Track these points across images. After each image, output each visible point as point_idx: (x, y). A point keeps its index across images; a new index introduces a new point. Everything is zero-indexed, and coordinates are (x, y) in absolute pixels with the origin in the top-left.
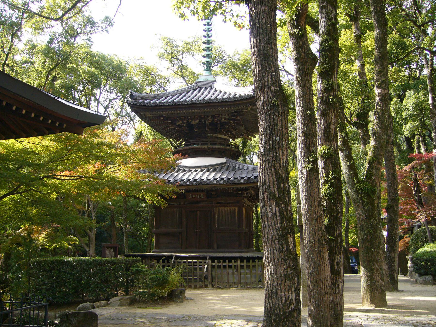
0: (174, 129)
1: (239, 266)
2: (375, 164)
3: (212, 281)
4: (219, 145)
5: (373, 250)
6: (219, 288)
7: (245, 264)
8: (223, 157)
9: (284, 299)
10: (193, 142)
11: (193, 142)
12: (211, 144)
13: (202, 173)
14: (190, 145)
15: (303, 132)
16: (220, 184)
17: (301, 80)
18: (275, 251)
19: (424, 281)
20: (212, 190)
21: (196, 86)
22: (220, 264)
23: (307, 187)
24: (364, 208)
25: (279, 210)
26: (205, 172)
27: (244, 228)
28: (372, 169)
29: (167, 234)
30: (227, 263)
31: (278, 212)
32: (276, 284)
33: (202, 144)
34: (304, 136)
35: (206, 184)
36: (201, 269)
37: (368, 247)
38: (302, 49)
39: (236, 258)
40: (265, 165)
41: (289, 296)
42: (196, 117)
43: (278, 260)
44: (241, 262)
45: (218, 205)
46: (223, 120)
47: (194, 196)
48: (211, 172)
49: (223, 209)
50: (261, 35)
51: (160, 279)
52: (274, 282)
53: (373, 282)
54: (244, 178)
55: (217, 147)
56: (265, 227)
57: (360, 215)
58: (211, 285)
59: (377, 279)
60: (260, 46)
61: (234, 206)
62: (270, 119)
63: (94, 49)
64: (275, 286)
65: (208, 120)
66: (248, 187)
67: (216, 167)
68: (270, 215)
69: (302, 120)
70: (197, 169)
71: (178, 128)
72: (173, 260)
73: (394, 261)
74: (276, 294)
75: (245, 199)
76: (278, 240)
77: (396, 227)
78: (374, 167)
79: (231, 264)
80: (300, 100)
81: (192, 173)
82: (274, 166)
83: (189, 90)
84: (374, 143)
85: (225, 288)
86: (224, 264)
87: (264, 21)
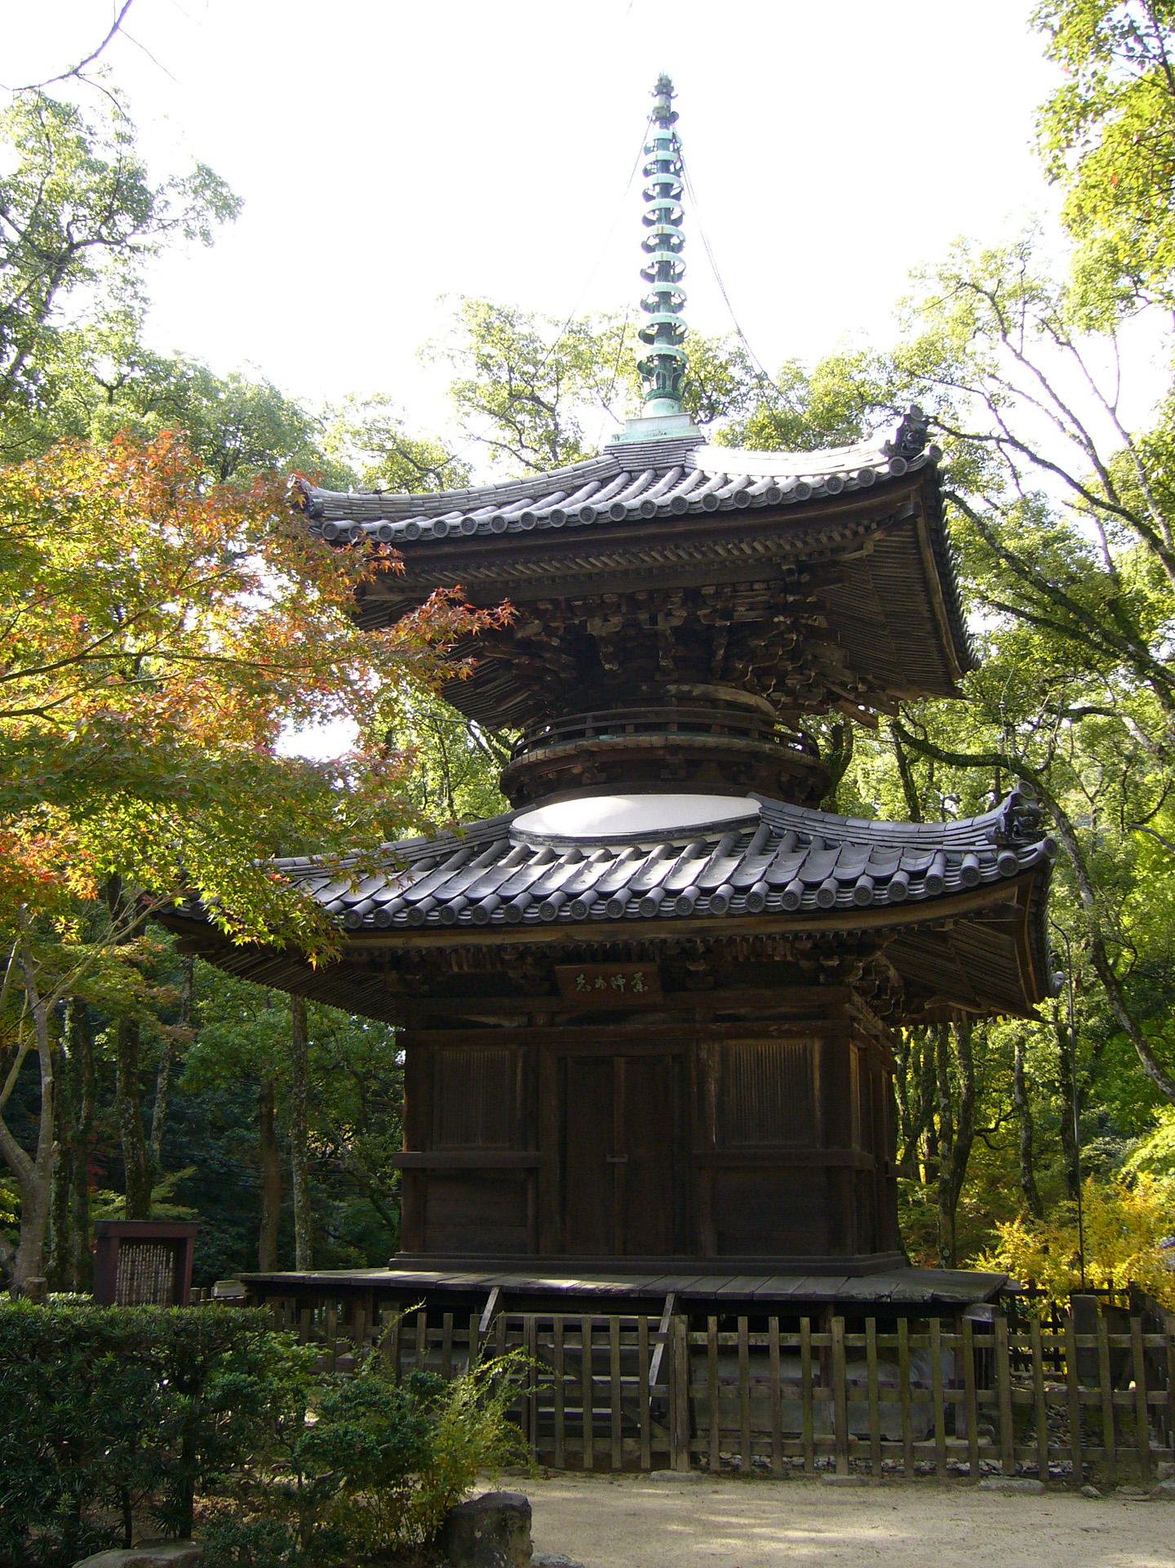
0: (507, 665)
1: (838, 1351)
3: (693, 1435)
4: (721, 734)
6: (732, 1473)
7: (869, 1339)
8: (743, 794)
10: (596, 719)
11: (596, 719)
12: (683, 727)
13: (637, 865)
14: (581, 734)
16: (730, 915)
20: (686, 952)
21: (608, 466)
22: (732, 1338)
26: (654, 861)
27: (856, 1147)
29: (464, 1176)
30: (773, 1336)
33: (641, 728)
35: (657, 918)
36: (633, 1363)
39: (817, 1310)
42: (610, 598)
44: (849, 1329)
45: (722, 1027)
46: (742, 612)
47: (600, 983)
48: (686, 861)
49: (745, 1049)
51: (366, 1452)
54: (855, 880)
55: (710, 740)
58: (685, 1457)
61: (800, 1034)
63: (157, 340)
65: (669, 614)
66: (878, 931)
67: (710, 839)
70: (614, 850)
71: (525, 660)
72: (487, 1314)
75: (857, 998)
79: (793, 1340)
81: (589, 866)
83: (578, 482)
85: (763, 1474)
86: (757, 1339)
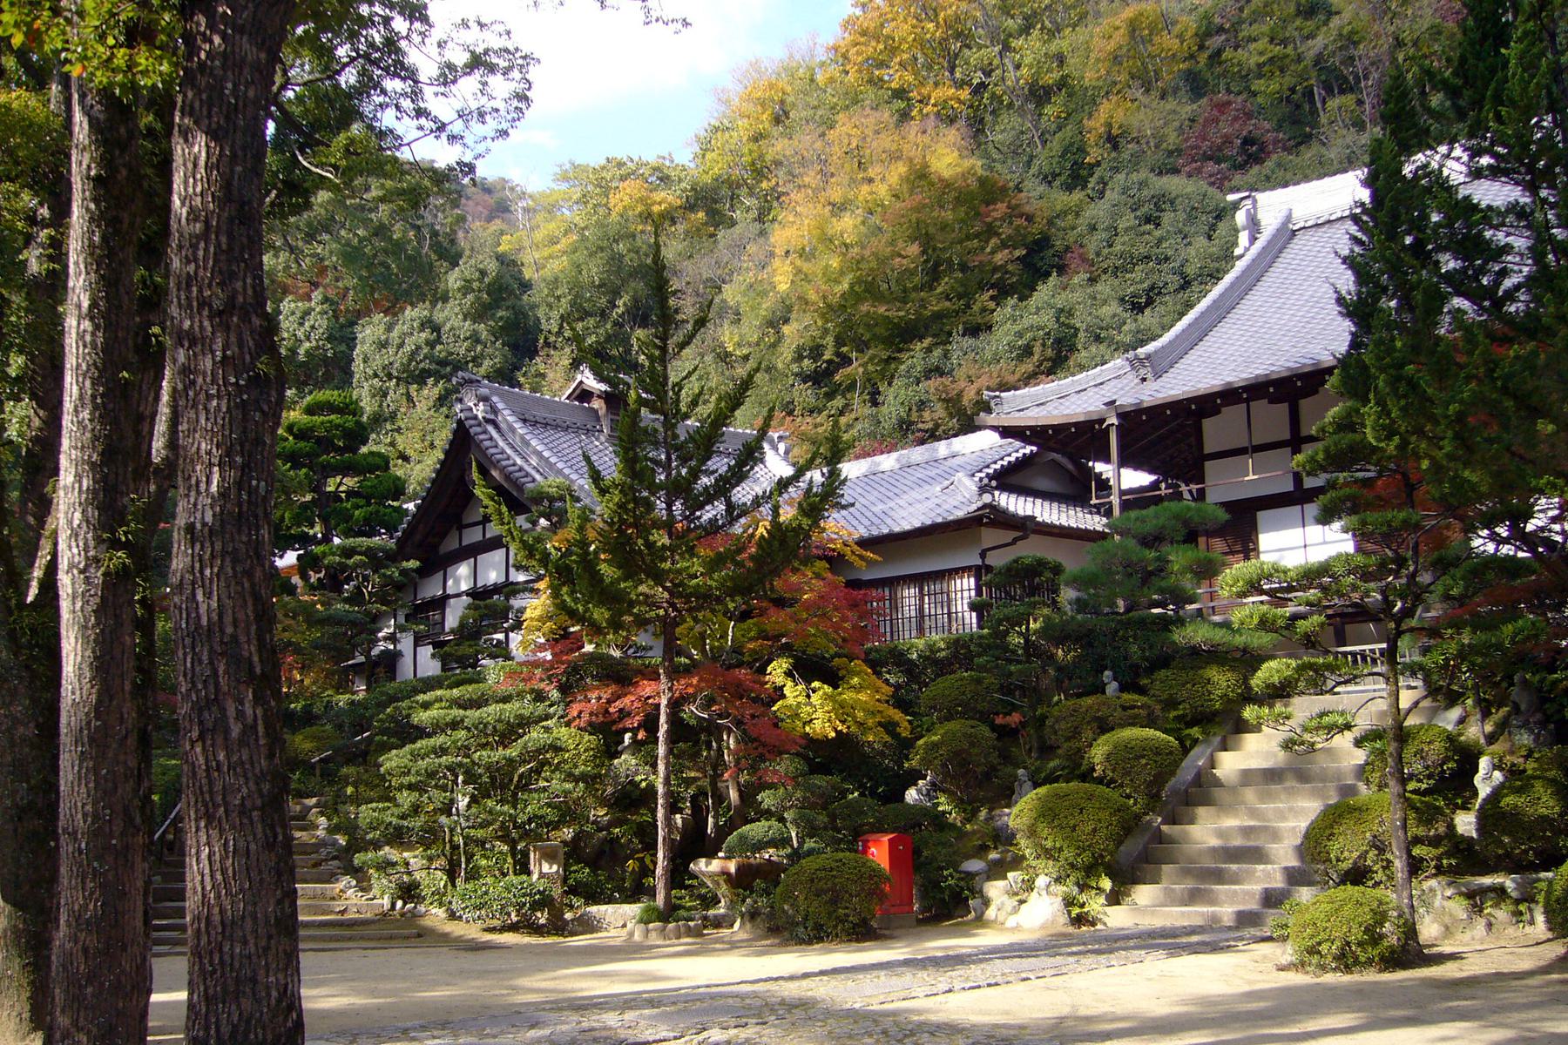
9: (274, 994)
15: (95, 438)
17: (108, 257)
18: (253, 847)
23: (102, 631)
25: (265, 715)
31: (260, 722)
32: (253, 950)
34: (102, 454)
38: (122, 151)
40: (221, 568)
41: (286, 985)
43: (260, 872)
50: (239, 134)
52: (245, 943)
56: (218, 769)
60: (232, 171)
62: (245, 419)
64: (249, 957)
68: (236, 730)
69: (94, 397)
74: (254, 980)
76: (262, 809)
80: (97, 327)
82: (249, 574)
87: (251, 93)
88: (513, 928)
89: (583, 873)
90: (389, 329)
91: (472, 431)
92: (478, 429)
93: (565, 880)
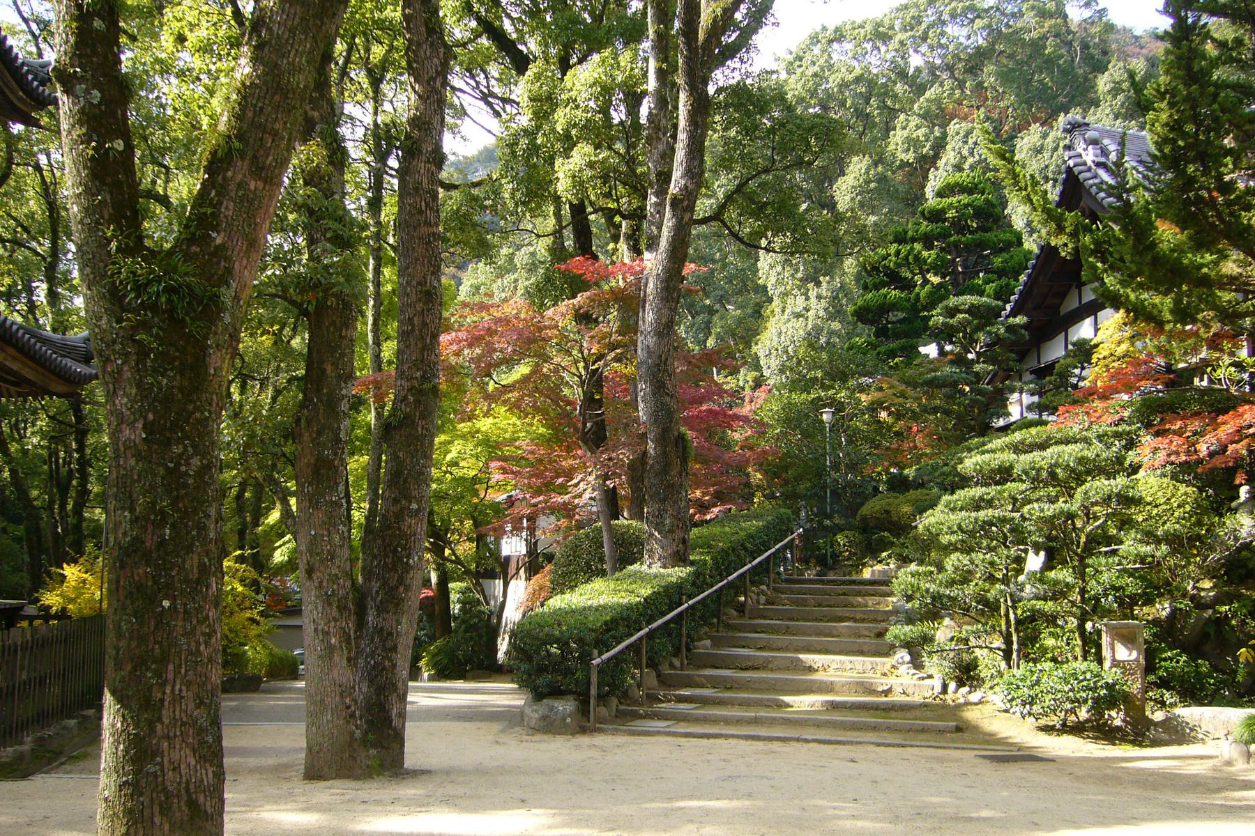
2: (238, 172)
5: (166, 604)
19: (544, 718)
24: (139, 385)
28: (219, 194)
37: (140, 587)
53: (151, 768)
57: (121, 420)
59: (175, 756)
73: (394, 649)
77: (414, 506)
78: (232, 187)
84: (247, 70)
88: (1077, 729)
89: (1175, 661)
90: (1045, 136)
91: (1080, 177)
92: (1088, 175)
93: (1150, 668)
